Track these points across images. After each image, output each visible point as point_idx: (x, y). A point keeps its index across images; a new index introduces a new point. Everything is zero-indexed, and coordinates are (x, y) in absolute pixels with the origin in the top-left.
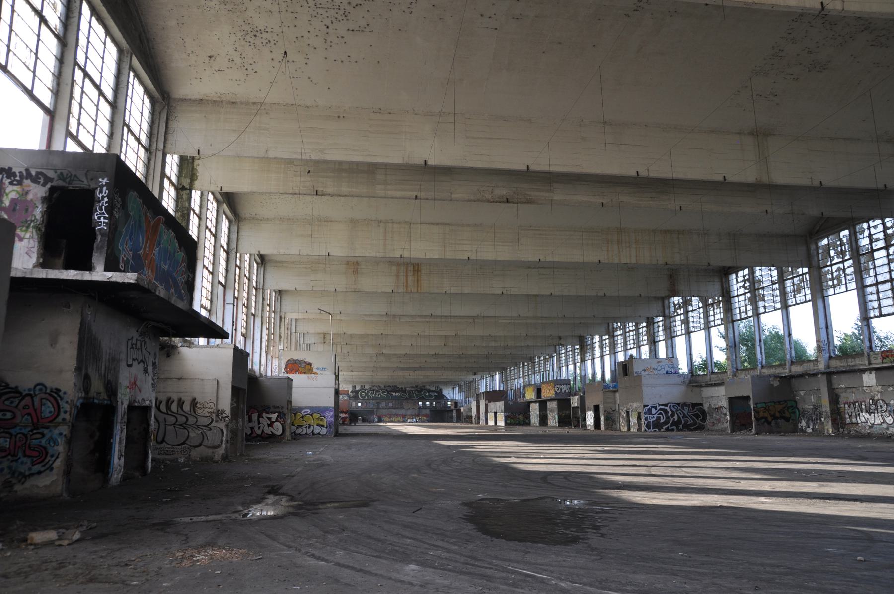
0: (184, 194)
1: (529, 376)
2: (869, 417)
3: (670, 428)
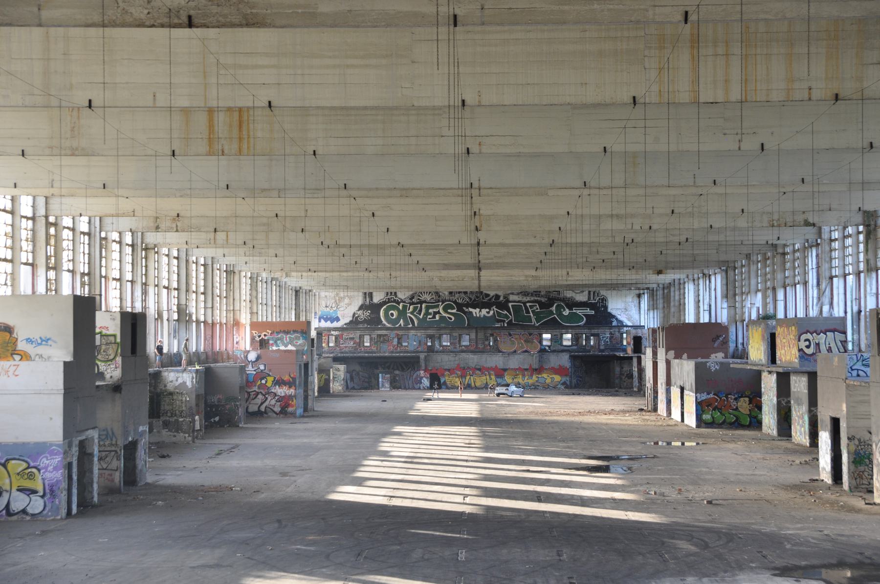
1: (774, 289)
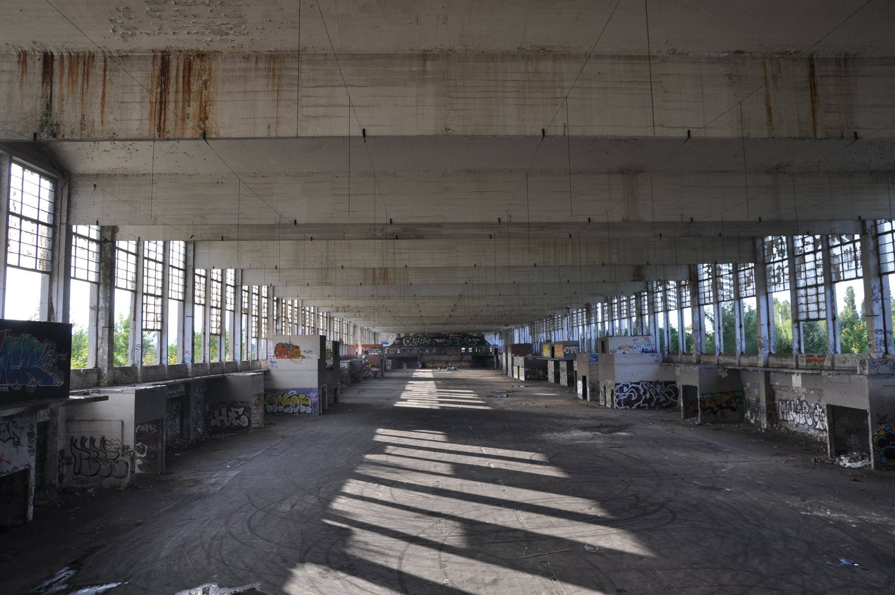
0: (107, 246)
1: (550, 331)
2: (796, 416)
3: (641, 405)
